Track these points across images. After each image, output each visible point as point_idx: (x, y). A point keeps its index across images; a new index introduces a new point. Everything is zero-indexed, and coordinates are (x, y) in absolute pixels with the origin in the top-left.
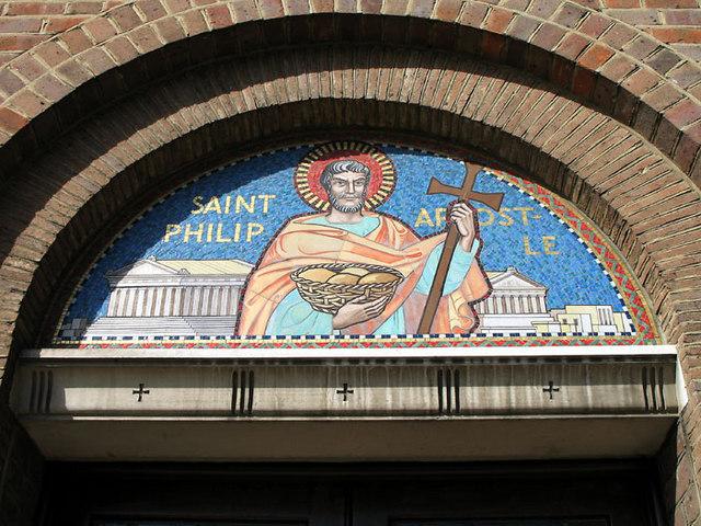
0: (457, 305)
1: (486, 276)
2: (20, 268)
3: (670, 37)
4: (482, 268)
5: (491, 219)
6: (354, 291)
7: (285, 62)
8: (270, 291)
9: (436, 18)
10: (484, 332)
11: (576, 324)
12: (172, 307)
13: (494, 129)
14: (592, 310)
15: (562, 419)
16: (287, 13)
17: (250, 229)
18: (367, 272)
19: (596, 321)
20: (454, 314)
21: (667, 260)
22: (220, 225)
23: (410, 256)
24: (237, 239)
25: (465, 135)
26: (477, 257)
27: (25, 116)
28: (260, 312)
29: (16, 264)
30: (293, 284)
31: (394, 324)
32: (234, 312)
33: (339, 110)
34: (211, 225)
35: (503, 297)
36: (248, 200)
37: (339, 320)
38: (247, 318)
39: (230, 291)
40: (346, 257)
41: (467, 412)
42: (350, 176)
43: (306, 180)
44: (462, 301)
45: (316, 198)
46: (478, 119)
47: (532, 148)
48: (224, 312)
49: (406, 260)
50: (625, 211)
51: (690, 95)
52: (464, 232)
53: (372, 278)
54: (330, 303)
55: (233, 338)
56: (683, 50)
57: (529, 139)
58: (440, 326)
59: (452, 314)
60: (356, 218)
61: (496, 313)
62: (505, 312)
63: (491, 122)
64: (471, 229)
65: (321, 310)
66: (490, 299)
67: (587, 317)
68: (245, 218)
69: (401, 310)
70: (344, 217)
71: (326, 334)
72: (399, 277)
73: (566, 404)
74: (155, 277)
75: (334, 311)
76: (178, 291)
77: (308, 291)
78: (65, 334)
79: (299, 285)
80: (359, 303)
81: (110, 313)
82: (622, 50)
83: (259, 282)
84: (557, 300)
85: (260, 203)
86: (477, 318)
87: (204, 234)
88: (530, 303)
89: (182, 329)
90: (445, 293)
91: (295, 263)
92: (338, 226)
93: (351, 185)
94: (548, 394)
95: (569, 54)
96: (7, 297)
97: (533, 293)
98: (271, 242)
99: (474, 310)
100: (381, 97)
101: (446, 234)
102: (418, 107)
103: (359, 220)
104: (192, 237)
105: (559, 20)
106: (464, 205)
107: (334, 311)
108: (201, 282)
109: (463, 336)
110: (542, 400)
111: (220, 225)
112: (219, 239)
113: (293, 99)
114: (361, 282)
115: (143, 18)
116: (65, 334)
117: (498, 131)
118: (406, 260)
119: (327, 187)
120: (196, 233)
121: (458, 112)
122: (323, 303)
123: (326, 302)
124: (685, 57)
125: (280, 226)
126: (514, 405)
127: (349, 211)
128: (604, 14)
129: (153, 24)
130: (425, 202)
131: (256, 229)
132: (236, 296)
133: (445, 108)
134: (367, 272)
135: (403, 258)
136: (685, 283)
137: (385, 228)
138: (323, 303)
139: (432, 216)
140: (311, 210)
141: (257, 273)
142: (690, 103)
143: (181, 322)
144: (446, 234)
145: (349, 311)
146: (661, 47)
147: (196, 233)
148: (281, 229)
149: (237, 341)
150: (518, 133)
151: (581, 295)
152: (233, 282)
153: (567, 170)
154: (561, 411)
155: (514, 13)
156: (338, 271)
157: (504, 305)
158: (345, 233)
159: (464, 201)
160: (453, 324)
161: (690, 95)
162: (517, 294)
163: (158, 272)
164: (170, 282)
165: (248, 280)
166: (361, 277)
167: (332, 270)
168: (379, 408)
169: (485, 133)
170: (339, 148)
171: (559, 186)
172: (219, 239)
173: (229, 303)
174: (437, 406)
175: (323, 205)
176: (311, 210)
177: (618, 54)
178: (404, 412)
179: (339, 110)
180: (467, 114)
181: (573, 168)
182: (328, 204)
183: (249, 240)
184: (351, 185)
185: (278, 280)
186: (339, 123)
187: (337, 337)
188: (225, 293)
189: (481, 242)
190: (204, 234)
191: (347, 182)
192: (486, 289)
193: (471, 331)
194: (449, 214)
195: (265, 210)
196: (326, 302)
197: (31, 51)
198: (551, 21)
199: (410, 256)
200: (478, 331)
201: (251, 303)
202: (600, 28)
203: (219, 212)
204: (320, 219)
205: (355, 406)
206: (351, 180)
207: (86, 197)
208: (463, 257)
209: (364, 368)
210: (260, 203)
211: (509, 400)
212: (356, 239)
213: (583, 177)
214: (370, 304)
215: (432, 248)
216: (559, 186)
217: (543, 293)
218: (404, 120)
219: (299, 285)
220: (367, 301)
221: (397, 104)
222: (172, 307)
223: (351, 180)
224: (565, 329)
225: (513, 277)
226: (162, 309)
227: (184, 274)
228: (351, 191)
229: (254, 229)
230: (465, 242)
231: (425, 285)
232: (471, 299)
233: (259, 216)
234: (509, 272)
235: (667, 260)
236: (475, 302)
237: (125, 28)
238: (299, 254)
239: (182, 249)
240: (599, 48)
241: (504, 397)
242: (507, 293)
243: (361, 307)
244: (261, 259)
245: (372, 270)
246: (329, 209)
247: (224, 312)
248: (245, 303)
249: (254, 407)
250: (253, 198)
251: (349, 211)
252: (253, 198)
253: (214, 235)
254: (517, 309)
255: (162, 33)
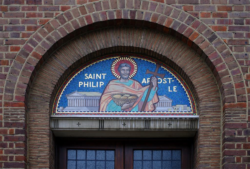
0: (151, 104)
1: (158, 97)
2: (47, 96)
3: (216, 29)
4: (157, 95)
5: (161, 81)
6: (127, 101)
7: (108, 33)
8: (106, 101)
9: (151, 21)
10: (156, 111)
11: (178, 109)
12: (83, 104)
13: (164, 56)
14: (182, 106)
15: (172, 131)
16: (108, 19)
17: (100, 83)
18: (129, 96)
19: (183, 109)
20: (150, 106)
21: (201, 95)
22: (93, 82)
23: (140, 92)
24: (97, 87)
25: (157, 57)
26: (156, 92)
27: (41, 54)
28: (104, 106)
29: (45, 95)
30: (111, 99)
31: (135, 110)
32: (98, 105)
33: (123, 48)
34: (90, 82)
35: (162, 103)
36: (99, 75)
37: (123, 108)
38: (101, 108)
39: (97, 100)
40: (124, 91)
41: (151, 129)
42: (125, 68)
43: (114, 69)
44: (152, 103)
45: (117, 75)
46: (160, 53)
47: (173, 62)
48: (95, 105)
49: (139, 93)
50: (194, 82)
51: (216, 50)
52: (154, 85)
53: (131, 97)
54: (121, 104)
55: (98, 112)
56: (219, 34)
57: (173, 60)
58: (146, 109)
59: (149, 106)
60: (127, 81)
61: (159, 106)
62: (162, 106)
63: (164, 54)
64: (156, 84)
65: (118, 105)
66: (159, 103)
67: (181, 108)
68: (99, 80)
69: (137, 105)
70: (124, 80)
71: (120, 111)
72: (137, 97)
73: (173, 127)
74: (78, 96)
75: (121, 106)
76: (84, 100)
77: (115, 100)
78: (59, 111)
79: (113, 99)
80: (127, 103)
81: (69, 105)
82: (202, 34)
83: (104, 98)
84: (174, 104)
85: (102, 76)
86: (155, 108)
87: (89, 85)
88: (168, 104)
89: (85, 109)
90: (148, 101)
91: (112, 93)
92: (123, 83)
93: (126, 71)
94: (169, 125)
95: (186, 35)
96: (45, 103)
97: (169, 102)
98: (106, 87)
99: (154, 106)
100: (134, 46)
101: (149, 86)
102: (144, 49)
103: (128, 81)
104: (86, 86)
105: (186, 23)
106: (155, 77)
107: (121, 106)
108: (89, 98)
109: (151, 112)
110: (167, 127)
111: (93, 82)
112: (93, 86)
113: (110, 46)
114: (128, 98)
115: (67, 20)
116: (59, 111)
117: (165, 57)
118: (139, 93)
119: (120, 72)
120: (87, 84)
121: (155, 51)
122: (119, 104)
123: (120, 103)
124: (219, 37)
125: (108, 83)
126: (161, 128)
127: (126, 79)
128: (199, 20)
129: (70, 22)
130: (145, 76)
131: (102, 84)
132: (98, 101)
133: (152, 50)
134: (129, 96)
135: (138, 92)
136: (204, 102)
137: (134, 84)
138: (119, 104)
139: (146, 80)
140: (116, 78)
141: (103, 96)
142: (216, 52)
143: (86, 108)
144: (149, 86)
145: (125, 106)
146: (213, 33)
147: (87, 84)
148: (108, 84)
149: (99, 113)
150: (170, 58)
151: (180, 102)
152: (97, 98)
153: (182, 69)
154: (172, 129)
155: (174, 20)
156: (122, 95)
157: (162, 105)
158: (124, 85)
159: (155, 76)
160: (149, 109)
161: (216, 50)
162: (163, 101)
163: (79, 95)
164: (82, 98)
165: (101, 98)
166: (128, 97)
167: (121, 95)
168: (131, 128)
169: (162, 57)
170: (123, 59)
171: (180, 72)
172: (93, 86)
173: (97, 103)
174: (144, 128)
175: (118, 77)
176: (116, 78)
177: (200, 35)
178: (137, 129)
179: (123, 48)
180: (158, 52)
181: (183, 69)
182: (120, 77)
183: (100, 87)
184: (126, 71)
185: (108, 98)
186: (123, 51)
187: (122, 112)
188: (96, 100)
189: (158, 88)
190: (89, 85)
191: (125, 70)
192: (158, 101)
193: (153, 111)
194: (150, 80)
195: (104, 78)
196: (120, 103)
197: (37, 31)
198: (183, 23)
199: (140, 92)
200: (155, 111)
201: (102, 103)
202: (196, 25)
203: (92, 78)
204: (118, 81)
205: (126, 128)
206: (126, 69)
207: (59, 77)
208: (153, 91)
209: (128, 119)
210: (102, 76)
211: (160, 127)
212: (127, 87)
213: (185, 72)
214: (130, 104)
215: (145, 89)
216: (180, 72)
217: (171, 102)
218: (140, 51)
219: (113, 99)
220: (129, 103)
221: (139, 48)
222: (83, 104)
223: (126, 69)
224: (175, 110)
225: (165, 97)
226: (81, 105)
227: (86, 96)
228: (126, 73)
229: (102, 84)
230: (154, 88)
231: (143, 99)
232: (154, 103)
233: (102, 80)
234: (164, 96)
235: (201, 95)
236: (155, 104)
237: (62, 24)
238: (113, 91)
239: (84, 89)
240: (195, 33)
241: (159, 126)
242: (163, 101)
243: (128, 104)
244: (104, 92)
245: (131, 95)
246: (120, 78)
247: (95, 105)
248: (101, 103)
249: (104, 128)
250: (101, 74)
251: (126, 79)
252: (101, 74)
253: (91, 85)
254: (165, 106)
255: (73, 25)
